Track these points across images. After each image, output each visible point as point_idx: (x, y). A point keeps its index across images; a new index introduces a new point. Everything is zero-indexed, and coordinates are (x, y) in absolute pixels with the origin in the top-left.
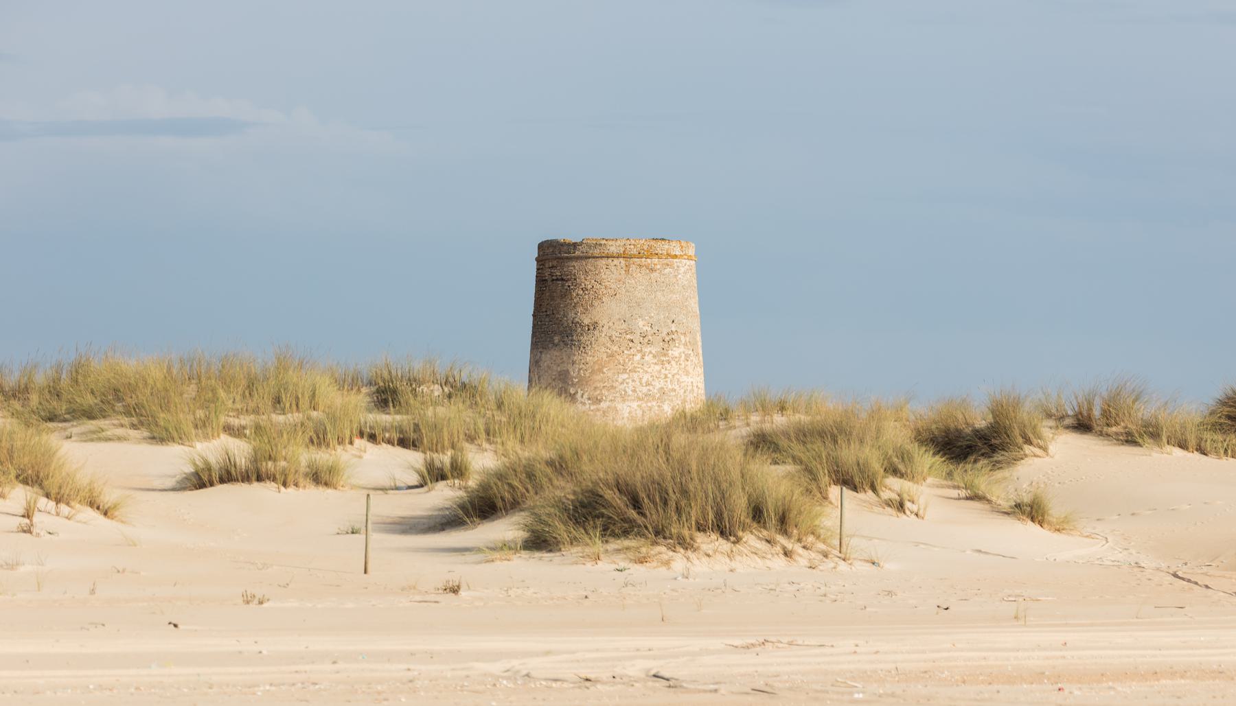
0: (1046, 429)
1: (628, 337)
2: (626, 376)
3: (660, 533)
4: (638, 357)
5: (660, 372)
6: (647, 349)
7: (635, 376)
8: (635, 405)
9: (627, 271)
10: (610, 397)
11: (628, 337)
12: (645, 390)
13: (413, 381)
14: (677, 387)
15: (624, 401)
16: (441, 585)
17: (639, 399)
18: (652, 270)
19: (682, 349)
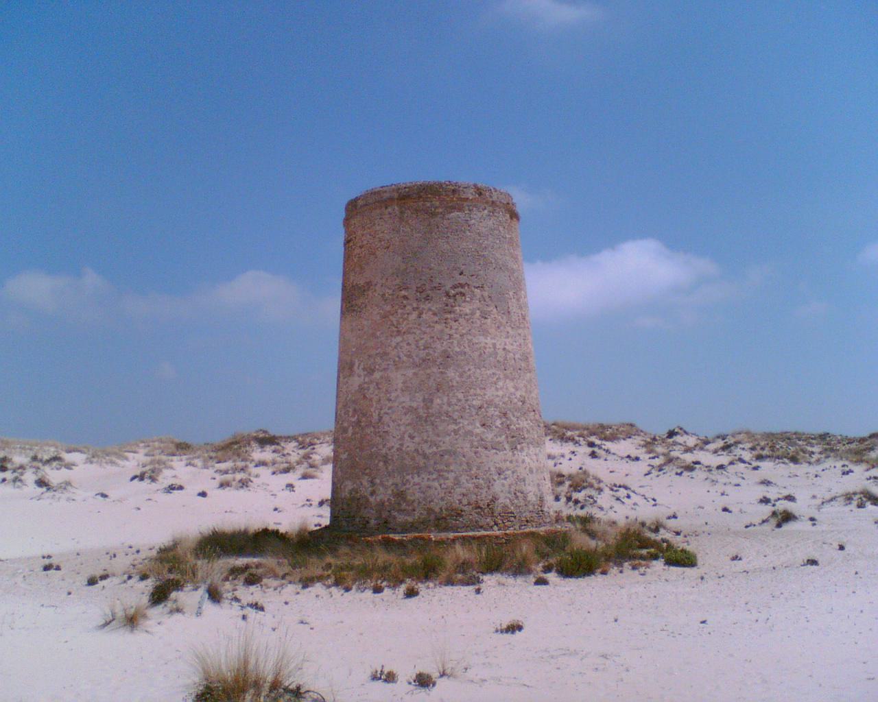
0: (146, 611)
1: (403, 293)
2: (399, 339)
3: (387, 548)
4: (414, 315)
5: (442, 331)
6: (425, 306)
7: (410, 338)
8: (410, 372)
9: (401, 219)
10: (383, 366)
11: (403, 293)
12: (422, 354)
13: (800, 516)
14: (467, 350)
15: (397, 369)
16: (640, 462)
17: (416, 365)
18: (433, 215)
19: (477, 304)
